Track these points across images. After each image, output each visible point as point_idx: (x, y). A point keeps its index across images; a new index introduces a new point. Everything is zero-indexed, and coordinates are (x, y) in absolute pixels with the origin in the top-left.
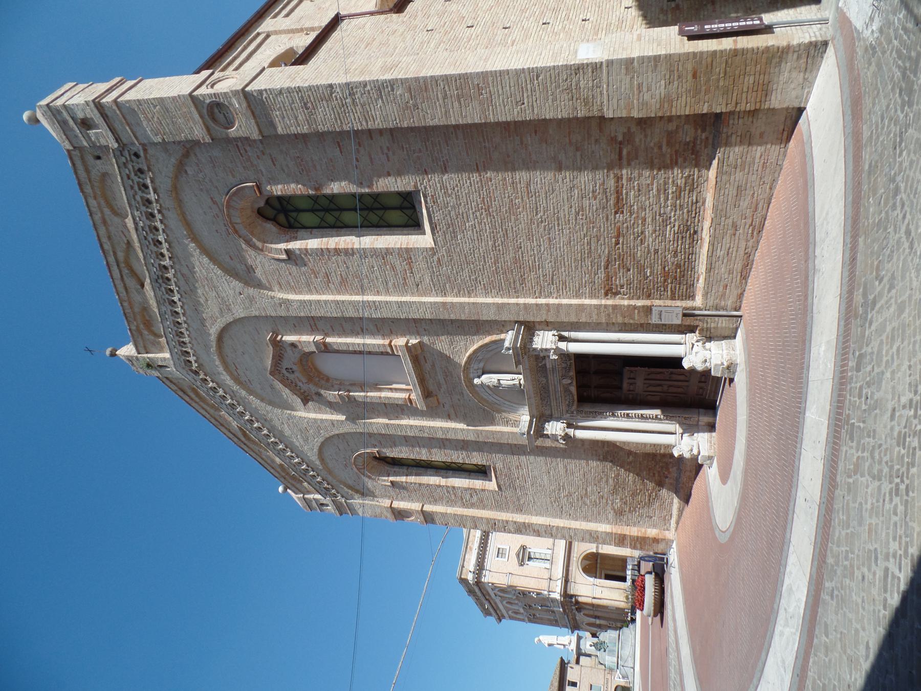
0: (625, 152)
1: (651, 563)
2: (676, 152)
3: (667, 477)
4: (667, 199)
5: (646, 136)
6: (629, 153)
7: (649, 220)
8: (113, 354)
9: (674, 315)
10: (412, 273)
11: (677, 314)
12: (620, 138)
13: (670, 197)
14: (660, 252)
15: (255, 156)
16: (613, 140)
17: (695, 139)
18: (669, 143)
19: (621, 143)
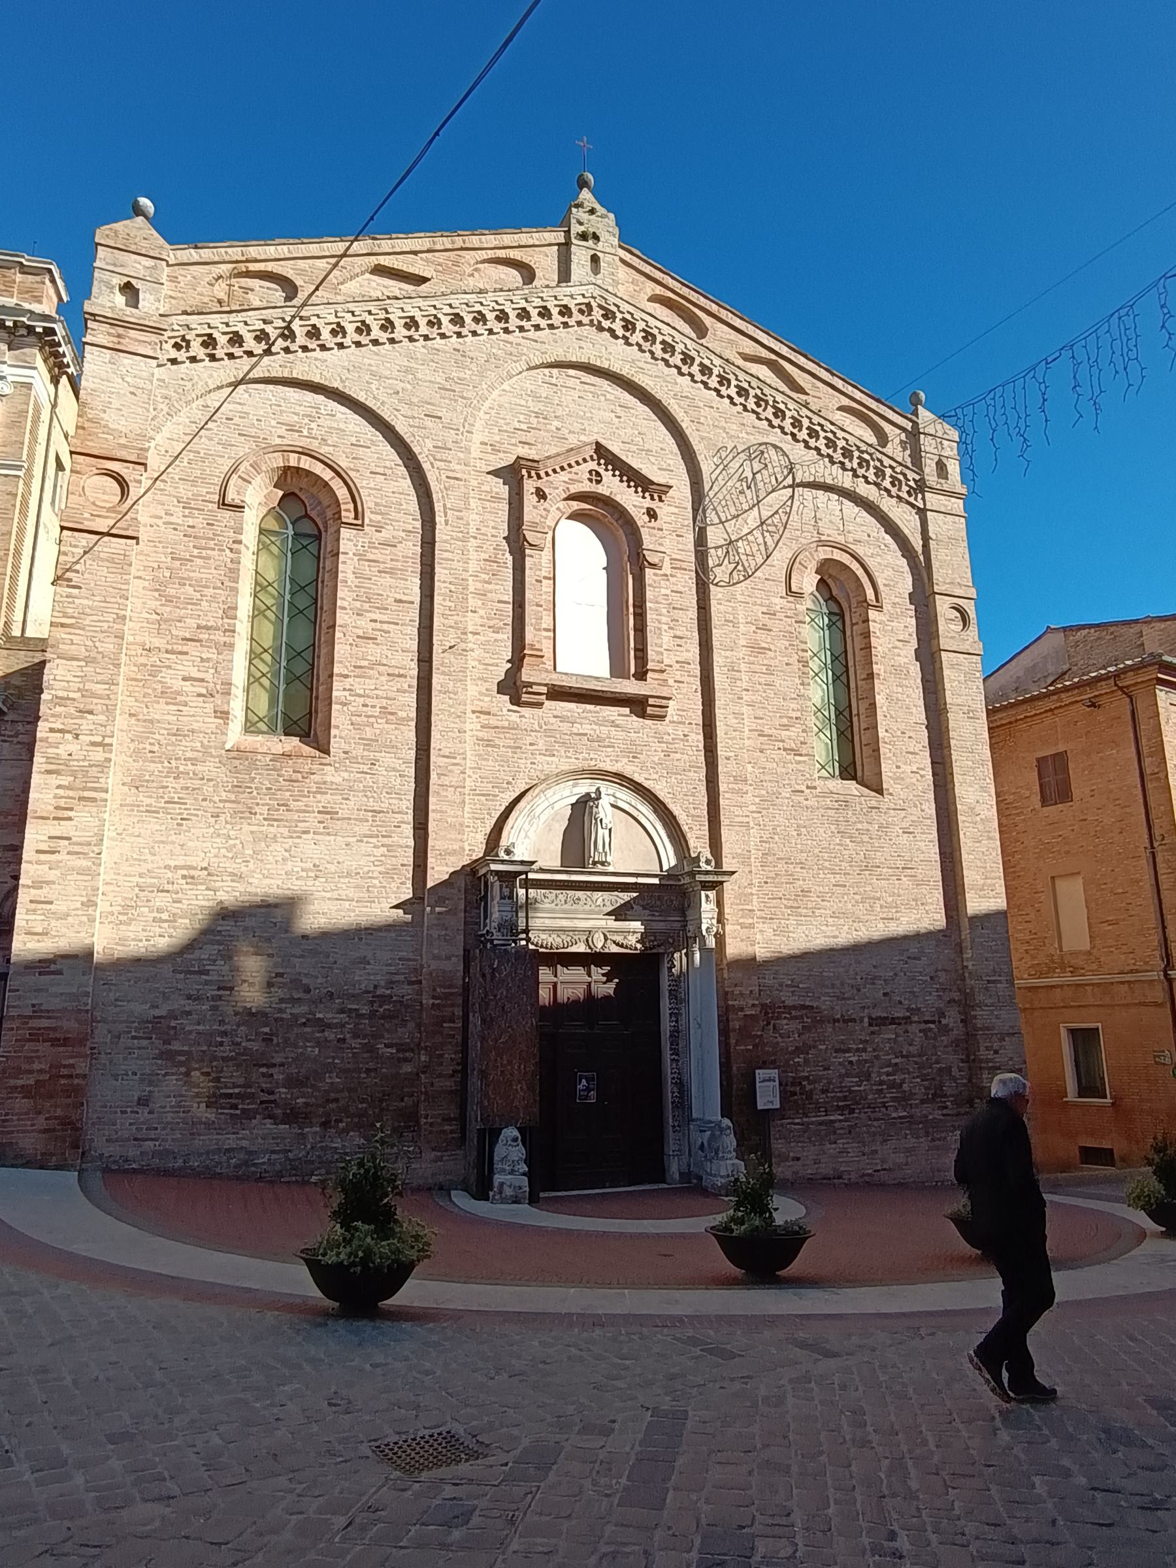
0: (932, 1026)
1: (1079, 881)
2: (933, 1079)
3: (325, 1125)
4: (888, 1074)
5: (946, 1047)
6: (930, 1030)
7: (864, 1056)
8: (583, 184)
9: (771, 1099)
10: (779, 749)
11: (772, 1102)
12: (944, 1022)
13: (891, 1078)
14: (825, 1073)
15: (384, 678)
16: (942, 1015)
17: (945, 1096)
18: (940, 1069)
19: (940, 1022)
